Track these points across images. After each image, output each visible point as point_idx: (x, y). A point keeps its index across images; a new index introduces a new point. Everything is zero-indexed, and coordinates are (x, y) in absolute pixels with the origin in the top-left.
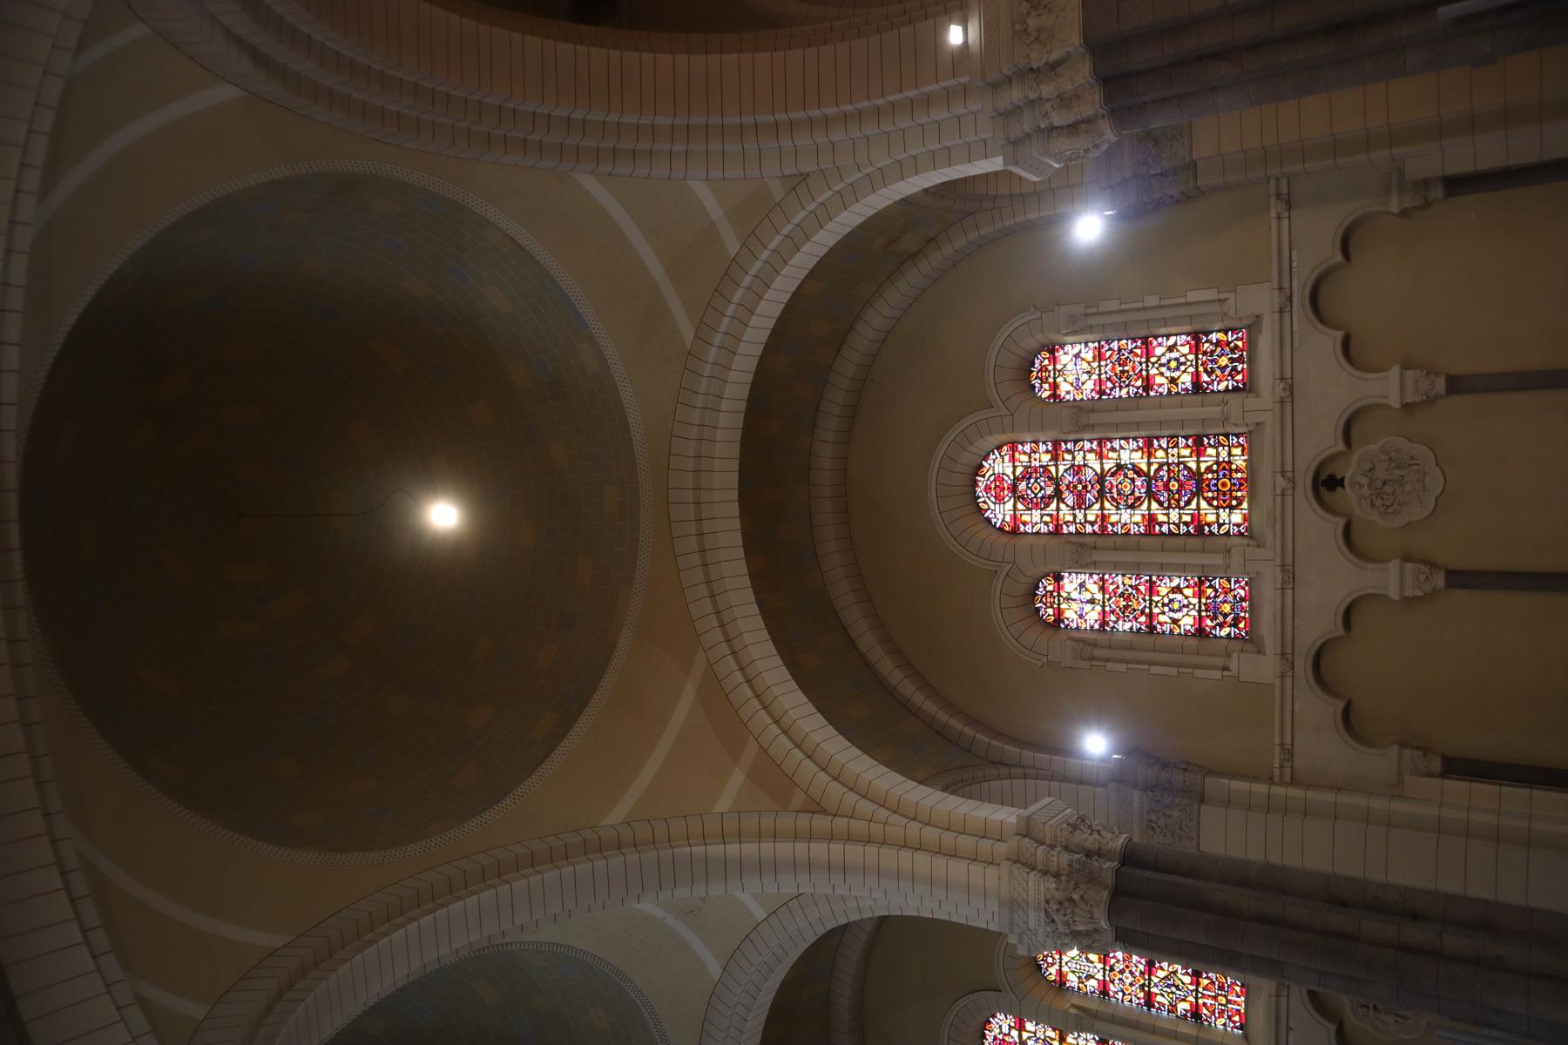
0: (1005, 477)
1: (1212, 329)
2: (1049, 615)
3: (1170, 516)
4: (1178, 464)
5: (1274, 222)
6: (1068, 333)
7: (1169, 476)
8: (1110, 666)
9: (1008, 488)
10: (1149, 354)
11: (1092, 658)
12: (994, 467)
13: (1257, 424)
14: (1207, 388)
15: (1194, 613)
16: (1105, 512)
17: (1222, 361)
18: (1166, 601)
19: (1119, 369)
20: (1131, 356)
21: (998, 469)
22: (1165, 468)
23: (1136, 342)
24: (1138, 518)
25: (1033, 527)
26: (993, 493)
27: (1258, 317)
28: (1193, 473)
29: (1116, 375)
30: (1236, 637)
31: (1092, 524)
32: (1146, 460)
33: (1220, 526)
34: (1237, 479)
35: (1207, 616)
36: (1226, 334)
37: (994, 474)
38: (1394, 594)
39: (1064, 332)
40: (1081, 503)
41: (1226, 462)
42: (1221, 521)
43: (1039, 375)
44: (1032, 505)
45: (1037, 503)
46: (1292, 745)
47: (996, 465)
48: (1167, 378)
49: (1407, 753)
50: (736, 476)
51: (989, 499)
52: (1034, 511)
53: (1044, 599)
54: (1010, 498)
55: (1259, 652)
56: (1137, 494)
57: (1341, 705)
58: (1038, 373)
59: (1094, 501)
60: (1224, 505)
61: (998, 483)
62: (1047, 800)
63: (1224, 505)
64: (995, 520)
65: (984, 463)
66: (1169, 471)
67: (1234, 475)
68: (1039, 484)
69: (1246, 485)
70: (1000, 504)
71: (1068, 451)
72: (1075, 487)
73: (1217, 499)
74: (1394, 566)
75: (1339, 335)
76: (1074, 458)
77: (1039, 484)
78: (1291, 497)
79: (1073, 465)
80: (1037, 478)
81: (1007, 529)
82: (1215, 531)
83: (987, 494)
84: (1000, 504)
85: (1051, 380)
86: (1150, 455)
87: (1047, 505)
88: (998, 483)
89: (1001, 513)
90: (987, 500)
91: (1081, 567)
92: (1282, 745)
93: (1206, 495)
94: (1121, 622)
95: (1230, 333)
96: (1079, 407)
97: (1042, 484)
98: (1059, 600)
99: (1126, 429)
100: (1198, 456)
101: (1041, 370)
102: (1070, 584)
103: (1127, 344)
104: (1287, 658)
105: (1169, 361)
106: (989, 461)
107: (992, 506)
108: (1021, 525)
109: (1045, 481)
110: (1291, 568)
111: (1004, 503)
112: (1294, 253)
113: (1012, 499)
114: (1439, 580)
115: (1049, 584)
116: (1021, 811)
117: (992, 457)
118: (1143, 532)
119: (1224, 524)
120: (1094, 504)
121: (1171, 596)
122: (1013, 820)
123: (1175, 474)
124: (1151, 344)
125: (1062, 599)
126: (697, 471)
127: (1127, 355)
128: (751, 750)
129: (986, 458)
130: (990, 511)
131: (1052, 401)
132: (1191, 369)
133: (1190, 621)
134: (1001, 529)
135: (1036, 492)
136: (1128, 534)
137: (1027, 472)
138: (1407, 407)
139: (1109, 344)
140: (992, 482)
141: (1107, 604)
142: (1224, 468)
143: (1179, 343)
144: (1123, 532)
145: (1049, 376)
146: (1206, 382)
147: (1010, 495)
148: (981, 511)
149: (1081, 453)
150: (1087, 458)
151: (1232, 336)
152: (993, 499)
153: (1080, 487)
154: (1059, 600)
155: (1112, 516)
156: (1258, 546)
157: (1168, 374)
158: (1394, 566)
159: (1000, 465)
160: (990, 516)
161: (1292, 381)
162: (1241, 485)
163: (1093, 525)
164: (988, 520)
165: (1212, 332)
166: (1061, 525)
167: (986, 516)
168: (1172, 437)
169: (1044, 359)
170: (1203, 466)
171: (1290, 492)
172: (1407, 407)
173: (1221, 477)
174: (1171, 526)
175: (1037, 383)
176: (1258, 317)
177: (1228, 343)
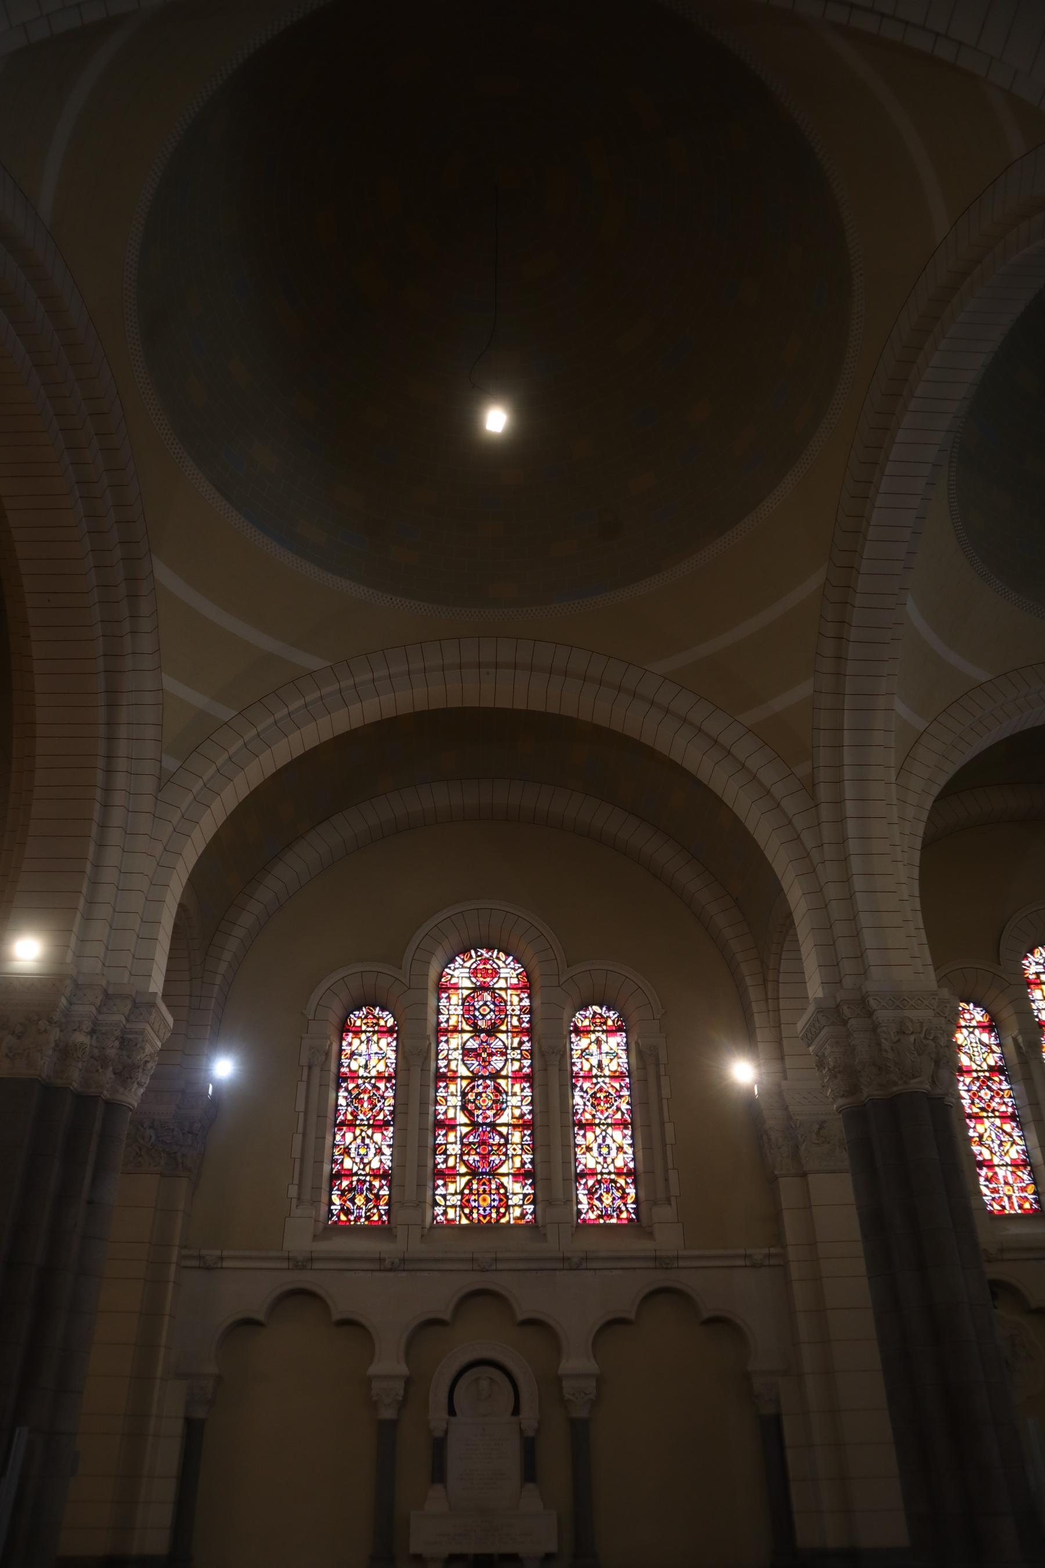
0: (495, 980)
1: (639, 1188)
2: (582, 1021)
3: (454, 1145)
4: (506, 1154)
5: (742, 1252)
6: (639, 1045)
7: (493, 1145)
8: (302, 1086)
9: (485, 982)
10: (615, 1125)
11: (310, 1068)
12: (507, 968)
13: (545, 1235)
14: (580, 1184)
15: (355, 1169)
16: (459, 1080)
17: (360, 1200)
18: (367, 1141)
19: (601, 1095)
20: (614, 1108)
21: (504, 972)
22: (502, 1141)
23: (390, 1115)
24: (451, 1114)
25: (445, 1006)
26: (481, 967)
27: (650, 1235)
28: (496, 1169)
29: (359, 1094)
30: (330, 1211)
31: (447, 1066)
32: (511, 1122)
33: (444, 1196)
34: (490, 1214)
35: (351, 1182)
36: (633, 1203)
37: (499, 968)
38: (373, 1370)
39: (639, 1041)
40: (466, 1052)
41: (507, 1202)
42: (448, 1197)
43: (598, 1016)
44: (467, 1004)
45: (469, 1010)
46: (496, 1270)
47: (508, 970)
48: (350, 1144)
49: (400, 1386)
50: (507, 705)
51: (474, 962)
52: (461, 1007)
53: (370, 1016)
54: (475, 984)
55: (315, 1236)
56: (476, 1112)
57: (260, 1317)
58: (600, 1014)
59: (471, 1069)
60: (505, 1200)
61: (490, 972)
62: (170, 1020)
63: (464, 1201)
64: (452, 968)
65: (511, 958)
66: (499, 1145)
67: (494, 1211)
68: (489, 1013)
69: (485, 1222)
70: (469, 973)
71: (521, 1043)
72: (485, 1050)
73: (471, 1193)
74: (403, 1369)
75: (632, 1316)
76: (513, 1049)
77: (489, 1013)
78: (378, 1268)
79: (506, 1048)
80: (494, 1011)
81: (443, 980)
82: (438, 1192)
83: (480, 960)
84: (469, 973)
85: (364, 1028)
86: (515, 1126)
87: (467, 1020)
88: (490, 972)
89: (460, 974)
90: (473, 960)
91: (640, 1054)
92: (222, 1258)
93: (475, 1182)
94: (346, 1094)
95: (634, 1206)
96: (564, 1054)
97: (488, 1017)
98: (370, 1032)
99: (427, 1101)
100: (513, 1175)
101: (602, 1017)
102: (615, 1042)
103: (389, 1106)
104: (301, 1264)
105: (608, 1146)
106: (512, 963)
107: (468, 964)
108: (447, 994)
109: (491, 1019)
110: (219, 1266)
111: (470, 978)
112: (620, 1272)
113: (474, 986)
114: (388, 1414)
115: (613, 1021)
116: (160, 994)
117: (517, 965)
118: (438, 1118)
119: (445, 1200)
120: (468, 1069)
121: (372, 1146)
122: (153, 988)
123: (496, 1151)
124: (386, 1130)
125: (369, 1034)
126: (479, 665)
127: (616, 1104)
128: (226, 713)
129: (516, 960)
130: (462, 963)
131: (572, 1028)
132: (599, 1169)
133: (591, 1164)
134: (441, 976)
135: (481, 1010)
136: (436, 1103)
137: (501, 1002)
138: (559, 1379)
139: (391, 1087)
140: (491, 965)
141: (600, 1080)
142: (501, 1200)
143: (383, 1157)
144: (438, 1098)
145: (368, 1026)
146: (341, 1183)
147: (478, 984)
148: (465, 951)
149: (519, 1057)
150: (515, 1062)
151: (632, 1208)
152: (474, 966)
153: (484, 1055)
154: (370, 1032)
155: (455, 1086)
156: (422, 1236)
157: (353, 1146)
158: (403, 1369)
159: (509, 972)
160: (457, 963)
161: (402, 1270)
162: (485, 1217)
163: (445, 1067)
164: (453, 961)
165: (636, 1188)
166: (446, 1035)
167: (457, 958)
168: (533, 1149)
169: (386, 1022)
170: (504, 1180)
171: (748, 1263)
172: (559, 1379)
173: (493, 1197)
174: (444, 1147)
175: (589, 1013)
176: (650, 1235)
177: (376, 1206)
